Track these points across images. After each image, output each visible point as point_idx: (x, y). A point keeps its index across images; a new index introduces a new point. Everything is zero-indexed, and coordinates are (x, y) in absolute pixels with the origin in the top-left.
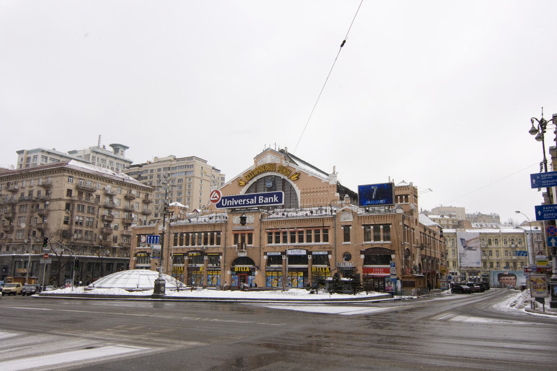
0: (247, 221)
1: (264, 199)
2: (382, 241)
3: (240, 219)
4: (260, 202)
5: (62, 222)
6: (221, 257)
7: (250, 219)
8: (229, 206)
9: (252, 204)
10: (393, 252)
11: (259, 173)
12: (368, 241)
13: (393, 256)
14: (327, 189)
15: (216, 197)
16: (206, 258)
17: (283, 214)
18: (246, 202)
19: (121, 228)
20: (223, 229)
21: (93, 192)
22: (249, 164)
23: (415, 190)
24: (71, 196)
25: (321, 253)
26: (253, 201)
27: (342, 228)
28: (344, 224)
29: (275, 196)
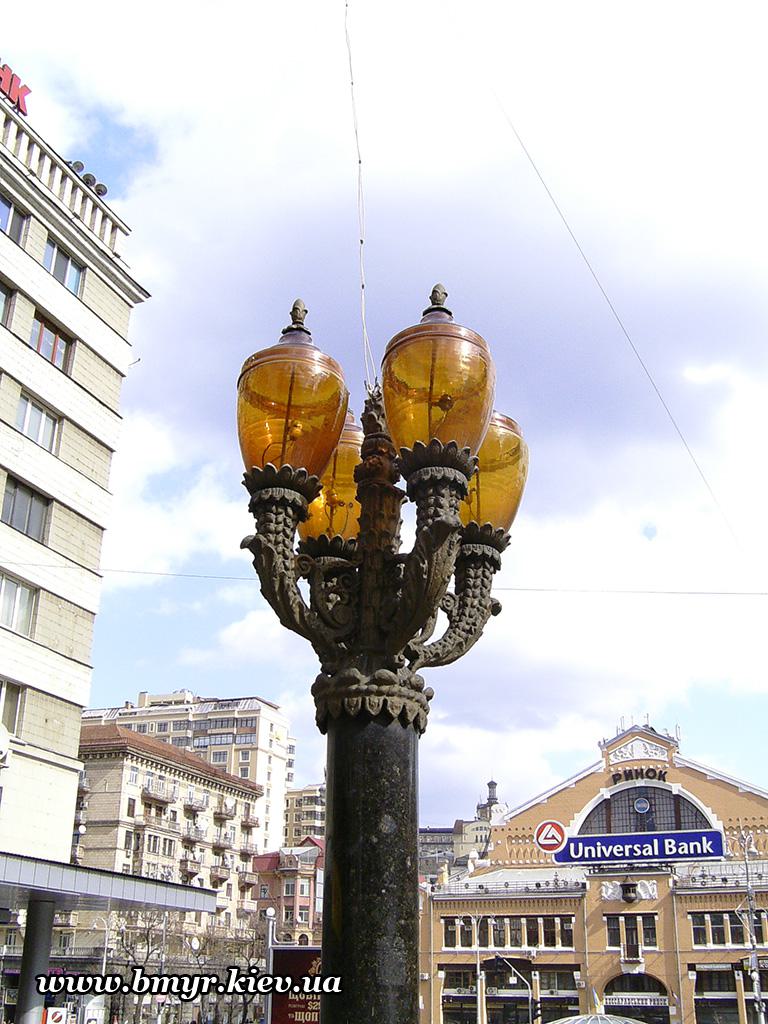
1: (677, 847)
3: (620, 890)
4: (667, 852)
7: (648, 890)
8: (590, 858)
9: (648, 857)
12: (516, 946)
15: (553, 837)
18: (632, 851)
24: (133, 816)
26: (648, 850)
29: (704, 839)
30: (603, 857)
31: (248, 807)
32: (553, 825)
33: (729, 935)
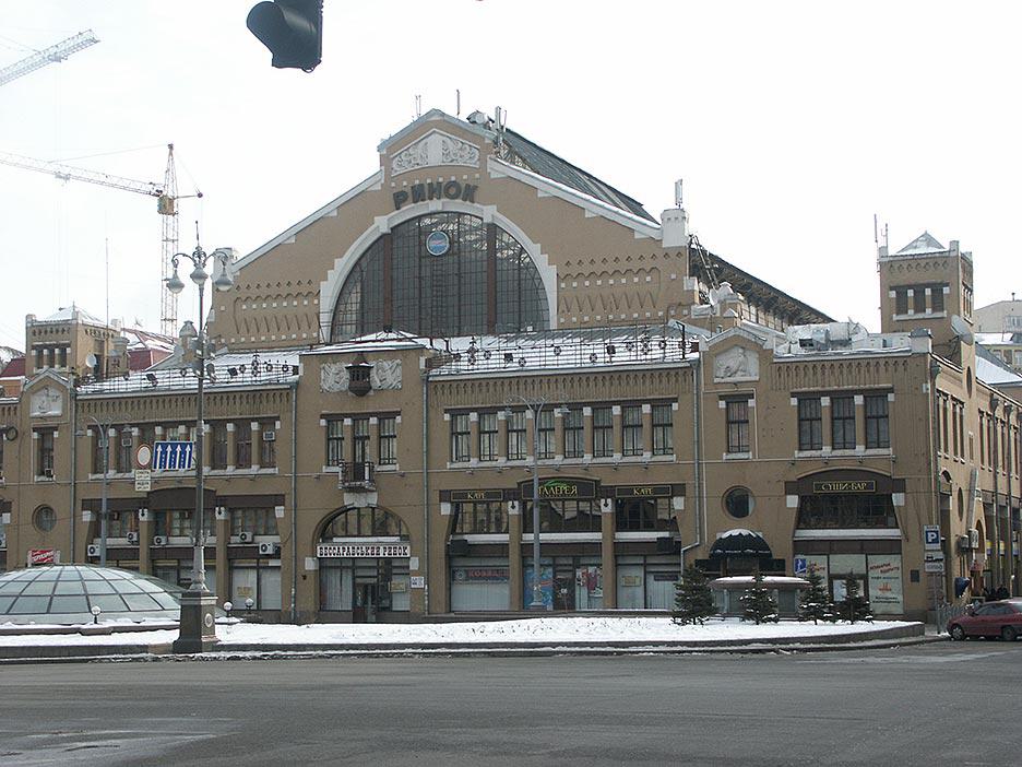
3: (346, 375)
6: (279, 512)
10: (900, 486)
13: (898, 499)
14: (653, 263)
17: (509, 357)
23: (966, 264)
27: (794, 401)
28: (41, 424)
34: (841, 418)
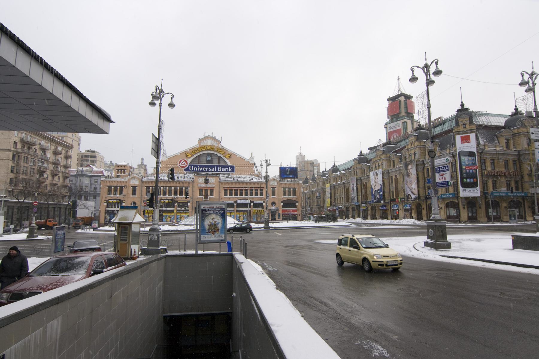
0: (210, 181)
2: (292, 197)
5: (10, 171)
7: (212, 180)
8: (195, 171)
10: (297, 202)
11: (202, 151)
13: (297, 204)
16: (176, 204)
19: (50, 178)
20: (191, 185)
21: (32, 145)
22: (194, 143)
24: (16, 148)
25: (259, 202)
30: (199, 171)
31: (67, 152)
32: (185, 161)
33: (254, 194)
34: (115, 190)
